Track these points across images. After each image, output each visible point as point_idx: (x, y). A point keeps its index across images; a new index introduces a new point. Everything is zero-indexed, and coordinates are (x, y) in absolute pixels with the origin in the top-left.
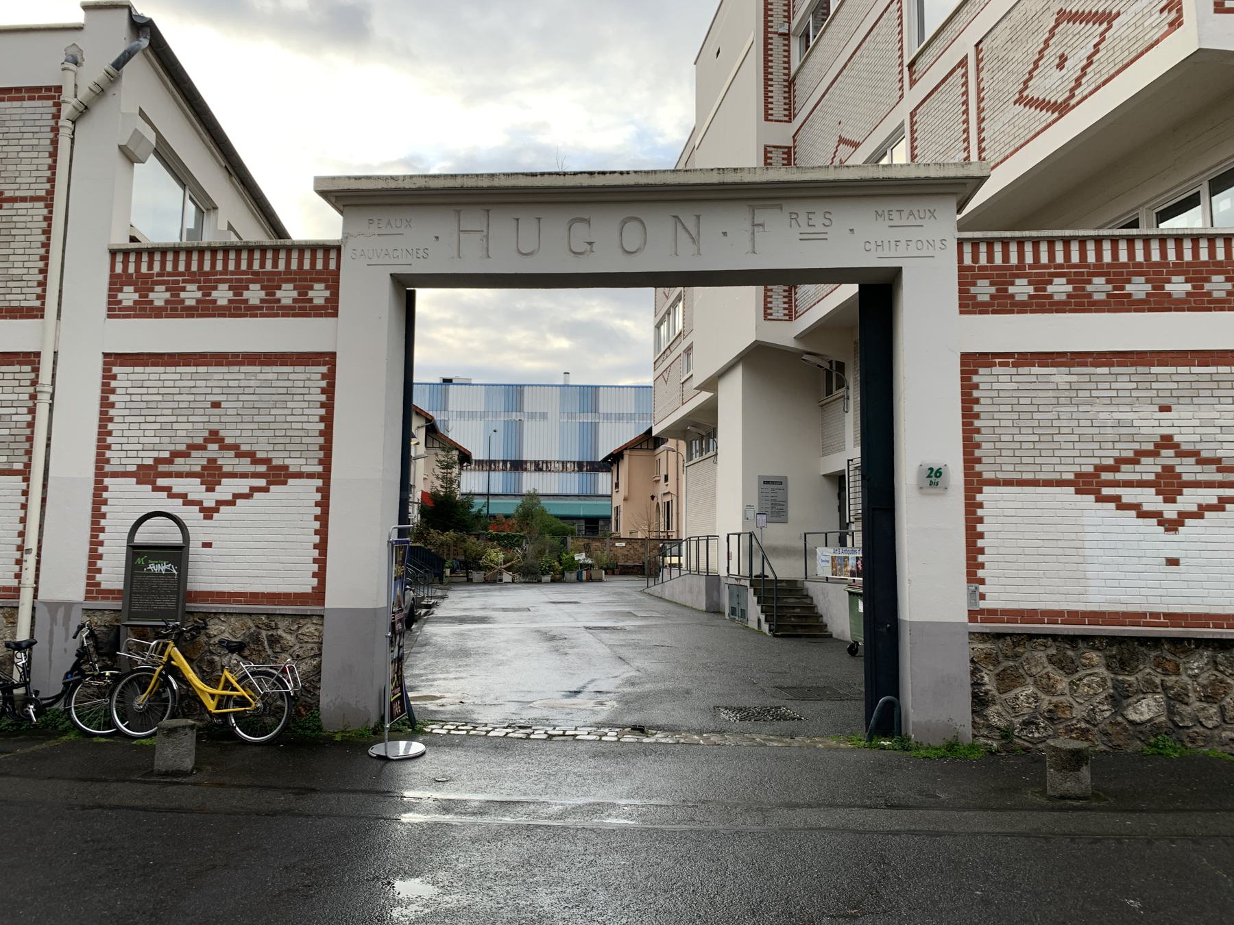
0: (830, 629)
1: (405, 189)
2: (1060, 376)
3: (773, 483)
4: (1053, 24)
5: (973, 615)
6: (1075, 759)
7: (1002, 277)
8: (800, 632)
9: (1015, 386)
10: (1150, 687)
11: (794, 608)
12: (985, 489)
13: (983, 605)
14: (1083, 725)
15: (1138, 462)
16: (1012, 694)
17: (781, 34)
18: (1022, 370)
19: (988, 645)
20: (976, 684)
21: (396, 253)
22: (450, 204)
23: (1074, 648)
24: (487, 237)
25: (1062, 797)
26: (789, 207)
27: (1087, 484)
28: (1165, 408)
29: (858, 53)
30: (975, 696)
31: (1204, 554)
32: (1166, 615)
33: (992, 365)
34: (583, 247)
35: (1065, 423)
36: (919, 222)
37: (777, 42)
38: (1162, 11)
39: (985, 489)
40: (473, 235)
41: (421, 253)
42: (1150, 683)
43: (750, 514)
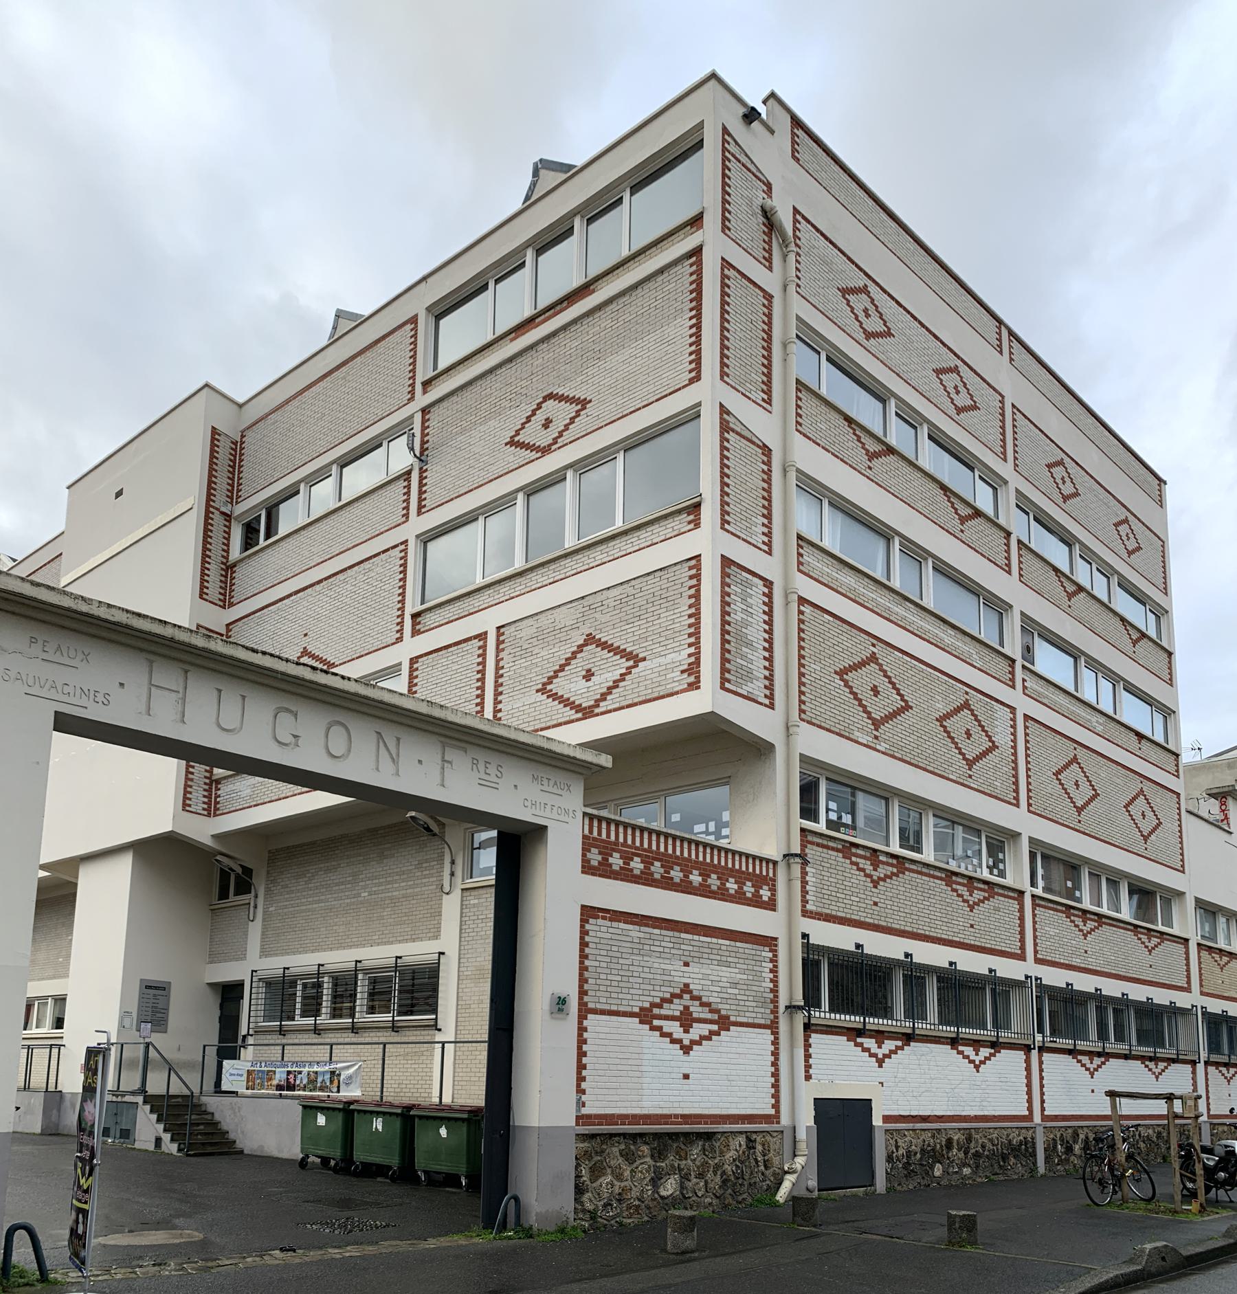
0: (239, 1145)
1: (99, 618)
2: (634, 931)
3: (156, 988)
4: (582, 642)
5: (581, 1119)
6: (690, 1224)
7: (607, 848)
8: (209, 1149)
9: (609, 936)
10: (673, 1170)
11: (198, 1124)
12: (589, 1016)
13: (584, 1111)
14: (637, 1203)
15: (671, 1002)
16: (598, 1183)
17: (223, 513)
18: (615, 924)
19: (586, 1144)
20: (578, 1177)
21: (66, 689)
22: (141, 650)
23: (635, 1143)
24: (184, 699)
25: (683, 1253)
26: (474, 752)
27: (645, 1016)
28: (686, 964)
29: (341, 577)
30: (577, 1186)
31: (702, 1071)
32: (683, 1116)
33: (597, 917)
34: (289, 739)
35: (635, 968)
36: (560, 792)
37: (218, 519)
38: (682, 672)
39: (589, 1016)
40: (166, 693)
41: (100, 698)
42: (672, 1166)
43: (127, 1023)
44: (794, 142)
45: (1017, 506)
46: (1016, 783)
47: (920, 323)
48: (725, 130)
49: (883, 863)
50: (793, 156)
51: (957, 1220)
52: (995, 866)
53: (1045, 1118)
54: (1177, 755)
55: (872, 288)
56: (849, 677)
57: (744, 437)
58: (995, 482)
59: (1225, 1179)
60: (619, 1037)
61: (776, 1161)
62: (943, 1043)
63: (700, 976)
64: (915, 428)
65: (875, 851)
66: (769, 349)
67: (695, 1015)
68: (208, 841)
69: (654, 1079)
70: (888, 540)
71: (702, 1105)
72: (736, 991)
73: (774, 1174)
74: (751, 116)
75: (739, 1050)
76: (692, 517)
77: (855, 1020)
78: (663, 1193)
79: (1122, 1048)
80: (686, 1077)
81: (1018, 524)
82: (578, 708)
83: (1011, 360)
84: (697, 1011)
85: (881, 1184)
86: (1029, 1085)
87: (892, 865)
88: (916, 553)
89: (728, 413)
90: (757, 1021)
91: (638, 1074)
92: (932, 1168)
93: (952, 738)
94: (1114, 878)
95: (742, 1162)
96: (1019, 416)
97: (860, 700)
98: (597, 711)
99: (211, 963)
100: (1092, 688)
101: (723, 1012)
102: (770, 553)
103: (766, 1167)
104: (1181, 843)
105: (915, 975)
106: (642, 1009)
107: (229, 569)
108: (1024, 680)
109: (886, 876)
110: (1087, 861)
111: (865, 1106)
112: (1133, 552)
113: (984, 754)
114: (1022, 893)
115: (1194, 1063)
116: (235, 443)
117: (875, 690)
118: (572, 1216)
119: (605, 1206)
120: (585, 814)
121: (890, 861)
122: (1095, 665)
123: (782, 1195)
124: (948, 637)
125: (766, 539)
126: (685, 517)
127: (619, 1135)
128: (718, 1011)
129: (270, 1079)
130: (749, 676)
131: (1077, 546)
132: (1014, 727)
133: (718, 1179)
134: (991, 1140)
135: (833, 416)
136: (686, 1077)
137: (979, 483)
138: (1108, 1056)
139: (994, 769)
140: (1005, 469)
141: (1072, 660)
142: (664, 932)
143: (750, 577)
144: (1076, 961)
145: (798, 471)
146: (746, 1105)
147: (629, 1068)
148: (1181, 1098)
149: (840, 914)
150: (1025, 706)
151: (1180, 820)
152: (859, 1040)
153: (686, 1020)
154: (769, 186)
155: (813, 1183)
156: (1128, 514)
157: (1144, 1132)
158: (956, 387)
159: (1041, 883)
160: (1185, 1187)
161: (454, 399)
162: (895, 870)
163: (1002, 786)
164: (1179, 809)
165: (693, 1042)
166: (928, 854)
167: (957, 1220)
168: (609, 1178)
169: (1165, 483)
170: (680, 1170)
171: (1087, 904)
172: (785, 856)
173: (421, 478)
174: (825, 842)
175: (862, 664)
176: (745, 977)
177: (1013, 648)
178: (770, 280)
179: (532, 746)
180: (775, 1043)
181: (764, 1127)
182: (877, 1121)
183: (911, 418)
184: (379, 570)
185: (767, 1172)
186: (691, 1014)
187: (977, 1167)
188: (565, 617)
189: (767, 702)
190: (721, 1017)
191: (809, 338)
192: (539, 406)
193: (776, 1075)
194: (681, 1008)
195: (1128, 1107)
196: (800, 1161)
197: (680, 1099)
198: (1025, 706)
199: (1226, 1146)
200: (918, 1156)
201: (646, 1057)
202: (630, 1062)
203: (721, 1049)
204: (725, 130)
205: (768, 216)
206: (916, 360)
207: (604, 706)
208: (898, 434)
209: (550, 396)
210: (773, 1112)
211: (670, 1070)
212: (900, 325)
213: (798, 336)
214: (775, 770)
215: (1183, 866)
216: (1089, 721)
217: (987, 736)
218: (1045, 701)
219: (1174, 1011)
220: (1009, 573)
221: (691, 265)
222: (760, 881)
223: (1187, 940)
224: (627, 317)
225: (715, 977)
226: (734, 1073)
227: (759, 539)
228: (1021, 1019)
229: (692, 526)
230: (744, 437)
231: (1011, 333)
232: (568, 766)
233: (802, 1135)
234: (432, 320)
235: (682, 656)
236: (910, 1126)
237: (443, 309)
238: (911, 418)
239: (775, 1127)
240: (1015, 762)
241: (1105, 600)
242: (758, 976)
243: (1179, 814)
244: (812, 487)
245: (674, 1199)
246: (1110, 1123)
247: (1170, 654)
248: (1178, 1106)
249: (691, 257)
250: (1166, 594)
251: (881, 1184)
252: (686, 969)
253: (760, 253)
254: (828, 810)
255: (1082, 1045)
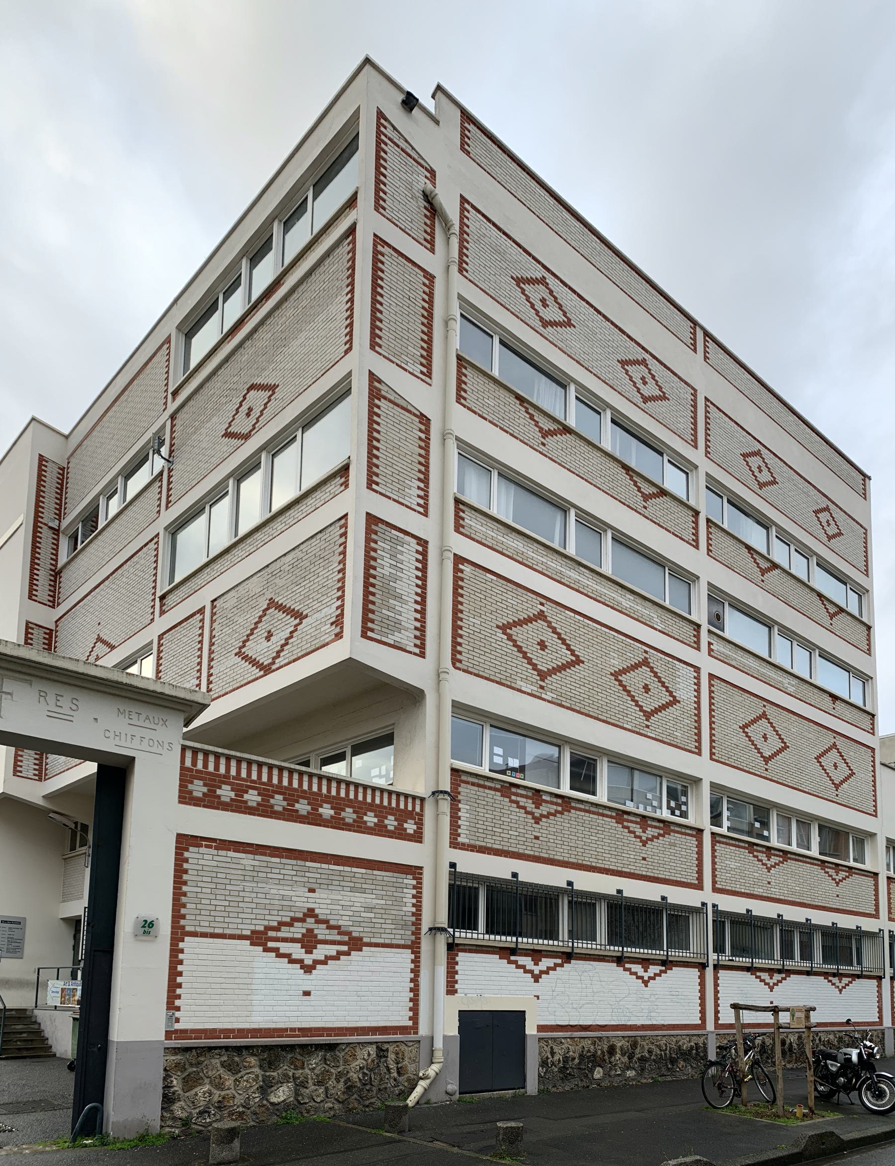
0: (54, 1050)
2: (247, 860)
3: (11, 922)
4: (265, 607)
5: (169, 1034)
8: (25, 1053)
9: (215, 864)
10: (286, 1078)
12: (186, 939)
14: (241, 1109)
16: (193, 1092)
17: (51, 528)
18: (221, 852)
19: (179, 1057)
20: (166, 1087)
23: (240, 1055)
26: (38, 685)
27: (258, 939)
28: (312, 890)
29: (120, 571)
30: (165, 1096)
31: (326, 988)
32: (300, 1029)
35: (247, 894)
37: (46, 534)
39: (186, 939)
44: (463, 135)
45: (707, 487)
46: (699, 734)
47: (604, 316)
48: (380, 115)
49: (546, 802)
50: (462, 148)
51: (501, 1132)
52: (678, 807)
53: (717, 1026)
54: (873, 716)
55: (550, 280)
56: (513, 631)
57: (398, 405)
58: (686, 467)
59: (844, 1084)
60: (223, 958)
61: (411, 1068)
62: (608, 961)
63: (329, 902)
64: (599, 413)
65: (538, 791)
66: (430, 326)
67: (320, 937)
68: (40, 802)
69: (266, 995)
70: (565, 512)
71: (325, 1019)
72: (372, 915)
73: (409, 1080)
74: (410, 102)
75: (372, 968)
76: (343, 480)
77: (508, 940)
78: (273, 1099)
79: (806, 965)
80: (307, 993)
81: (702, 500)
82: (261, 667)
83: (706, 358)
84: (321, 932)
85: (532, 1086)
86: (703, 998)
87: (556, 804)
88: (592, 525)
89: (380, 381)
90: (394, 942)
91: (247, 992)
92: (592, 1071)
93: (629, 692)
94: (805, 821)
95: (371, 1070)
96: (712, 409)
97: (525, 653)
98: (274, 667)
99: (64, 901)
100: (782, 652)
101: (354, 934)
102: (426, 514)
103: (399, 1073)
104: (875, 791)
105: (583, 904)
106: (253, 932)
107: (56, 574)
108: (710, 644)
109: (549, 814)
110: (776, 805)
111: (519, 1017)
112: (834, 536)
113: (663, 707)
114: (700, 831)
115: (879, 978)
116: (63, 469)
117: (542, 645)
118: (158, 1123)
119: (201, 1113)
120: (184, 748)
121: (555, 800)
122: (788, 633)
123: (412, 1100)
124: (627, 601)
125: (422, 502)
126: (339, 480)
127: (221, 1048)
128: (349, 933)
129: (74, 996)
130: (397, 626)
131: (774, 528)
132: (698, 684)
133: (341, 1086)
134: (659, 1047)
135: (502, 393)
136: (307, 993)
137: (668, 466)
138: (789, 972)
139: (675, 721)
140: (696, 456)
141: (767, 629)
142: (284, 861)
143: (401, 535)
144: (758, 891)
145: (458, 439)
146: (378, 1018)
147: (236, 986)
148: (787, 1010)
149: (495, 846)
150: (709, 666)
151: (874, 771)
152: (513, 958)
153: (309, 942)
154: (432, 172)
155: (453, 1086)
156: (829, 503)
157: (824, 1037)
158: (643, 378)
159: (726, 823)
160: (816, 1089)
161: (191, 403)
162: (560, 809)
163: (683, 734)
164: (873, 761)
165: (542, 972)
166: (602, 796)
167: (501, 1132)
168: (206, 1088)
169: (870, 478)
170: (295, 1078)
171: (775, 842)
172: (433, 793)
173: (170, 477)
174: (481, 782)
175: (529, 620)
176: (383, 902)
177: (700, 613)
178: (432, 262)
179: (107, 680)
180: (416, 961)
181: (399, 1037)
182: (531, 1030)
183: (591, 402)
184: (142, 562)
185: (401, 1079)
186: (316, 936)
187: (643, 1070)
188: (254, 586)
189: (417, 651)
190: (352, 939)
191: (473, 317)
192: (245, 397)
193: (415, 990)
194: (304, 931)
195: (748, 1017)
196: (435, 1068)
197: (299, 1014)
198: (709, 666)
199: (846, 1054)
200: (577, 1061)
201: (257, 976)
202: (237, 981)
203: (349, 968)
204: (380, 115)
205: (428, 198)
206: (599, 350)
207: (279, 662)
208: (574, 416)
209: (252, 387)
210: (410, 1023)
211: (287, 987)
212: (582, 317)
213: (462, 315)
214: (425, 714)
215: (875, 811)
216: (781, 682)
217: (667, 691)
218: (733, 663)
219: (860, 934)
220: (697, 547)
221: (349, 244)
222: (403, 816)
223: (876, 874)
224: (304, 303)
225: (341, 903)
226: (364, 989)
227: (414, 501)
228: (701, 938)
229: (343, 487)
230: (398, 405)
231: (707, 334)
232: (158, 702)
233: (439, 1044)
234: (182, 339)
235: (331, 611)
236: (568, 1034)
237: (191, 327)
238: (591, 402)
239: (412, 1037)
240: (698, 715)
241: (805, 579)
242: (400, 902)
243: (874, 766)
244: (471, 455)
245: (289, 1105)
246: (734, 1031)
247: (869, 628)
248: (784, 1018)
249: (348, 237)
250: (867, 575)
251: (532, 1086)
252: (311, 895)
253: (421, 235)
254: (492, 754)
255: (758, 962)
